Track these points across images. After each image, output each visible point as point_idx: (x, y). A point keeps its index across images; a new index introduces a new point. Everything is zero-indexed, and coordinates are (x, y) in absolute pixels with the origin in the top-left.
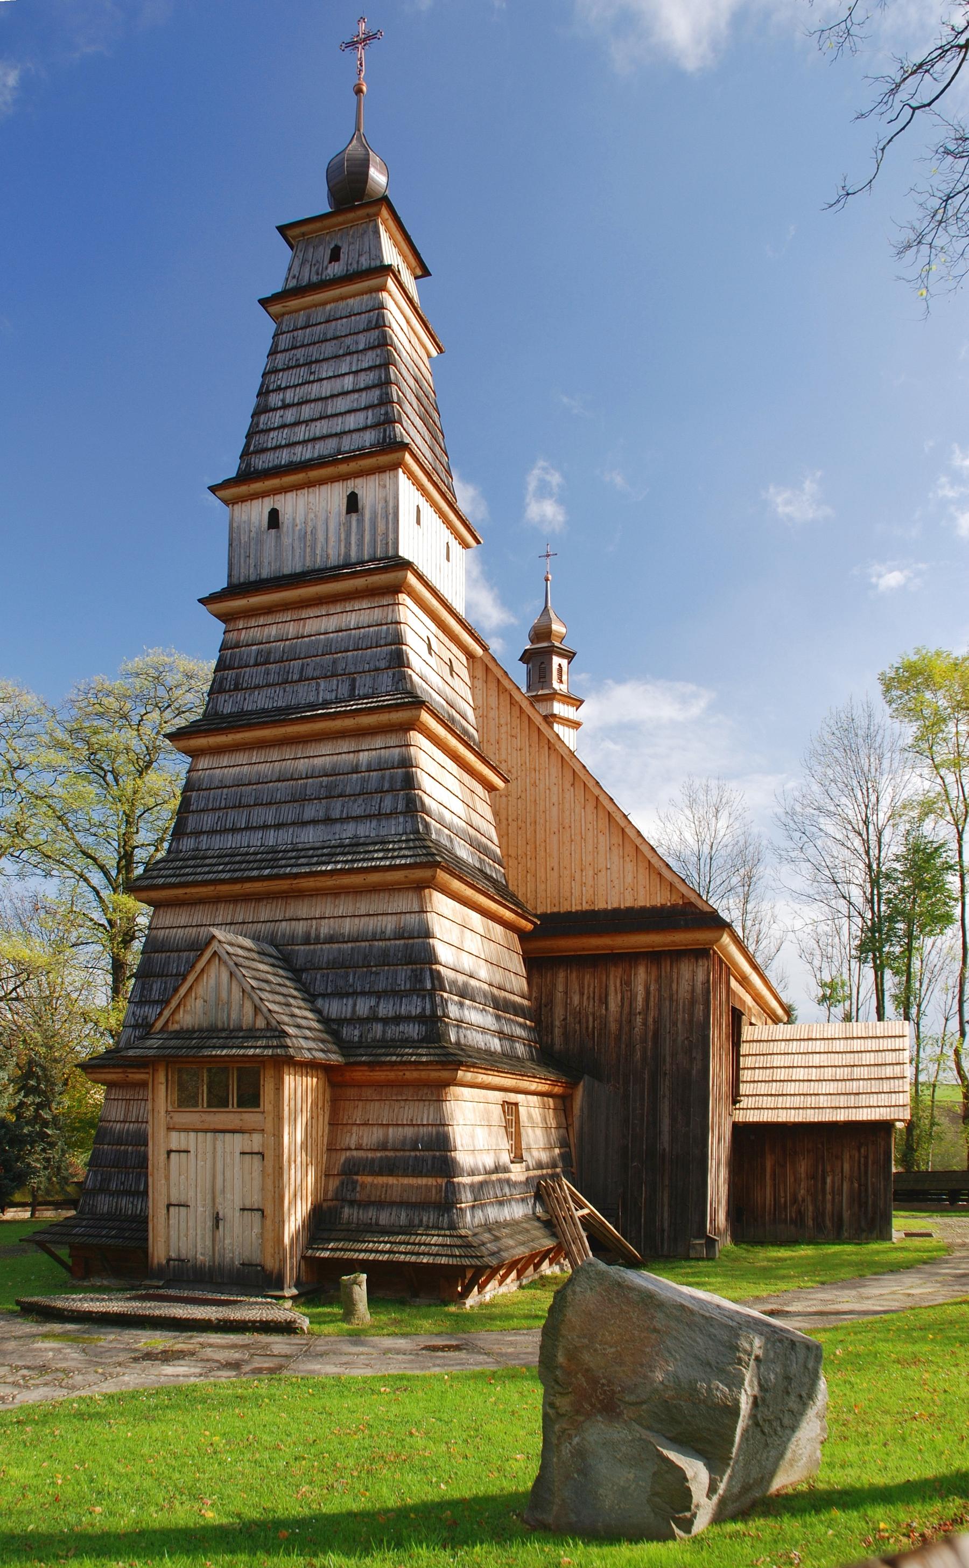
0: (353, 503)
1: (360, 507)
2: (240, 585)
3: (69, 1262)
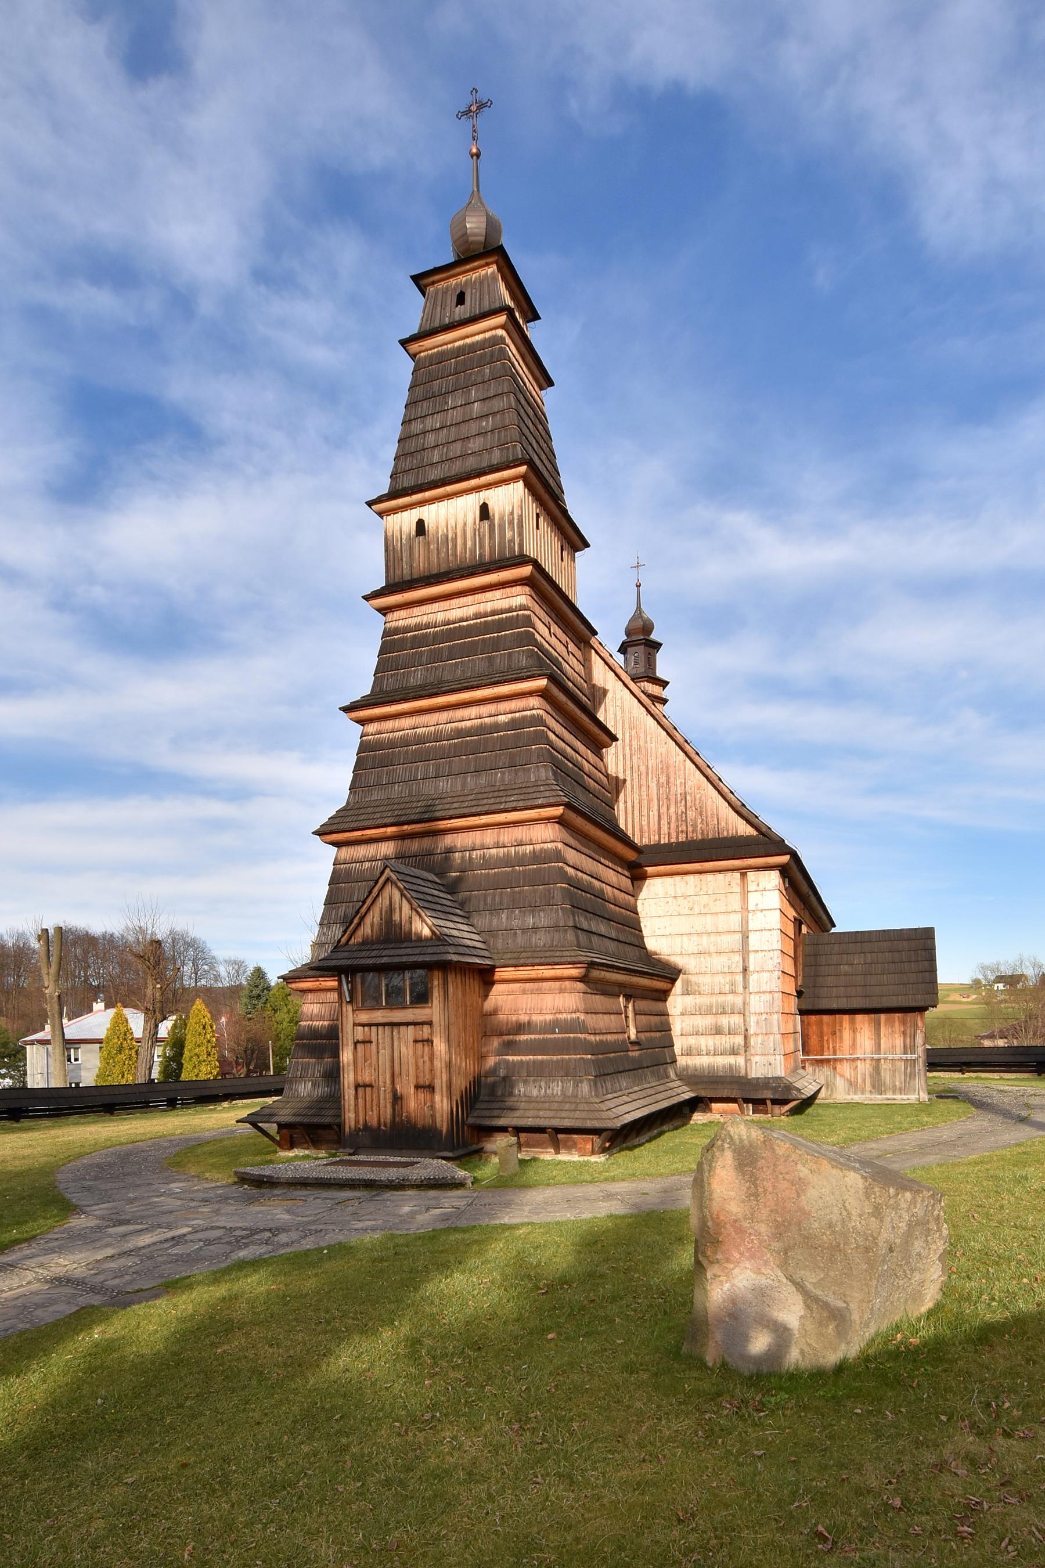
1: (491, 514)
2: (396, 585)
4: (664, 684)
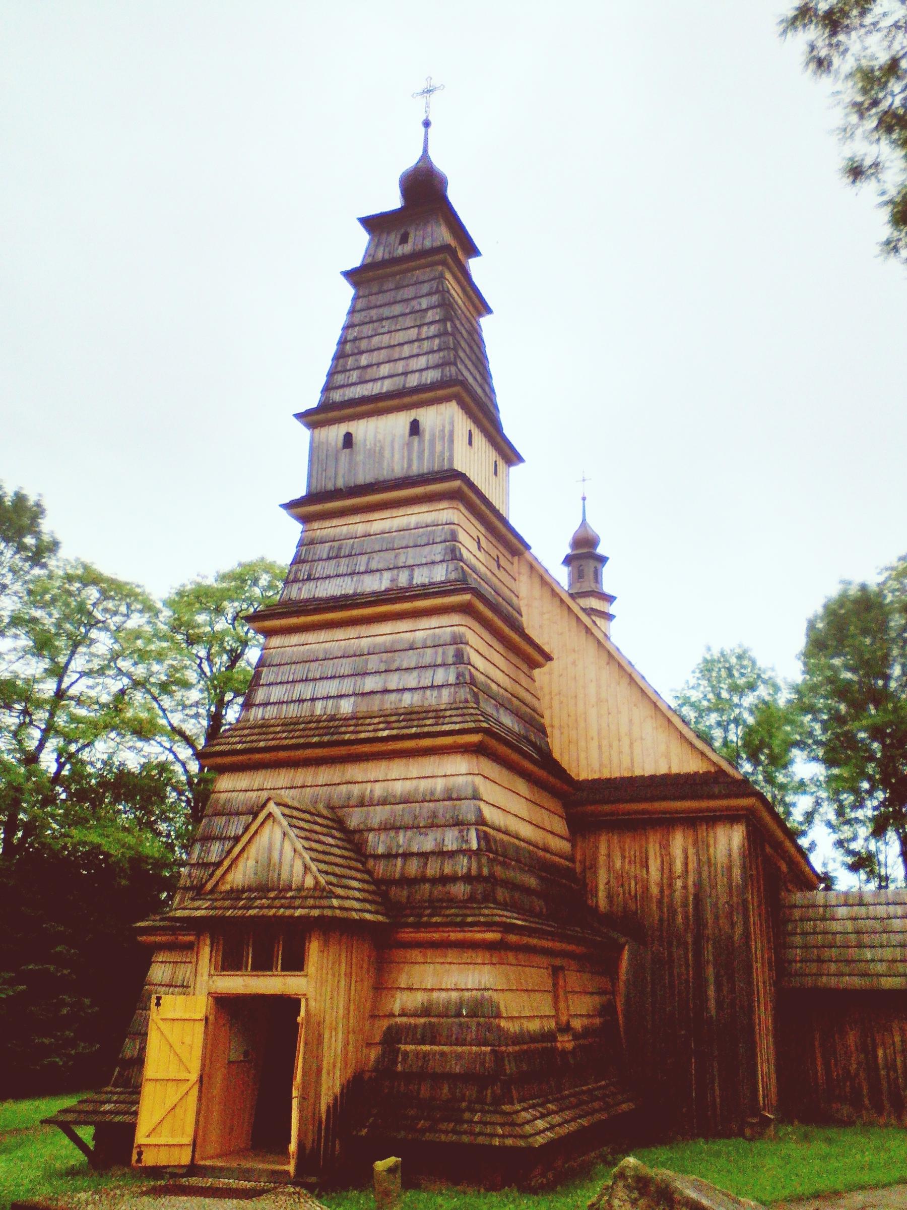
0: (415, 428)
1: (421, 428)
3: (91, 1144)
4: (610, 599)
